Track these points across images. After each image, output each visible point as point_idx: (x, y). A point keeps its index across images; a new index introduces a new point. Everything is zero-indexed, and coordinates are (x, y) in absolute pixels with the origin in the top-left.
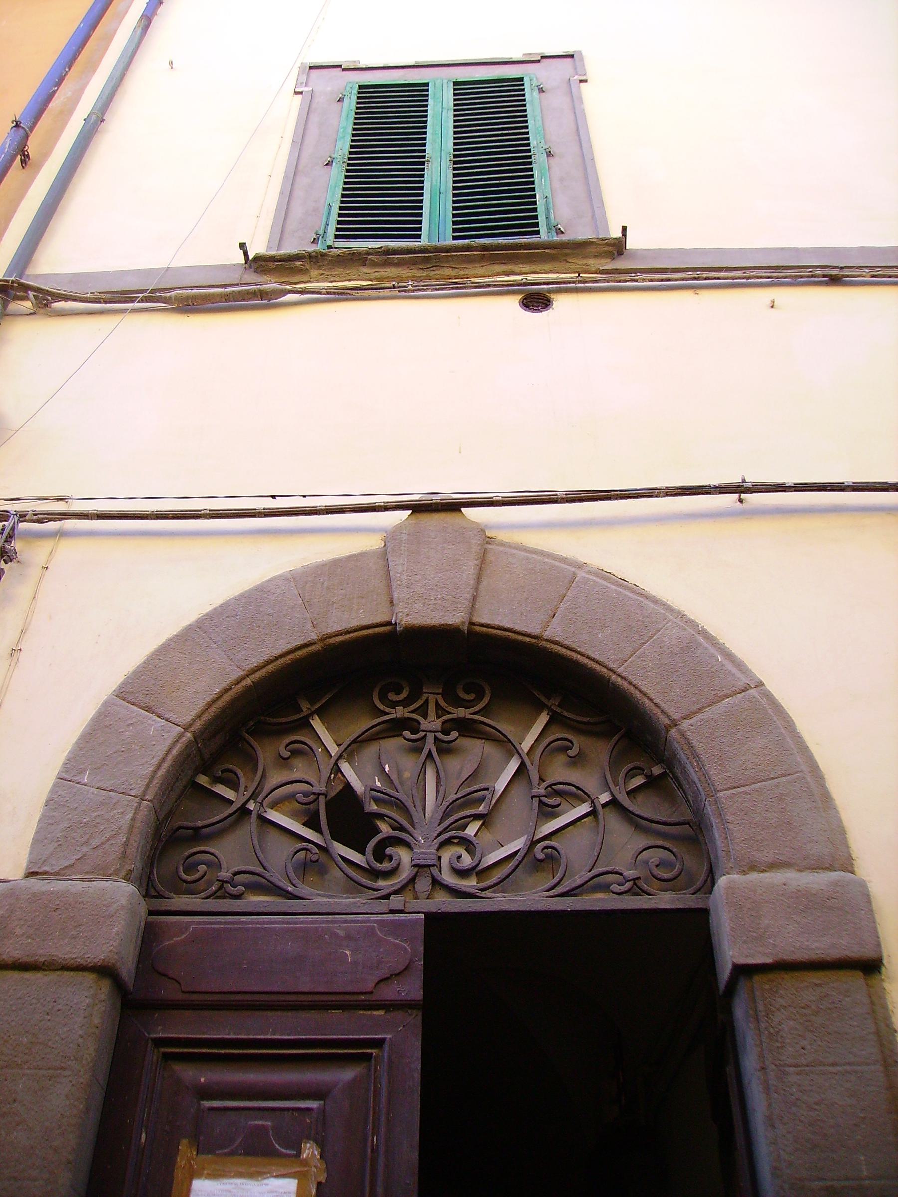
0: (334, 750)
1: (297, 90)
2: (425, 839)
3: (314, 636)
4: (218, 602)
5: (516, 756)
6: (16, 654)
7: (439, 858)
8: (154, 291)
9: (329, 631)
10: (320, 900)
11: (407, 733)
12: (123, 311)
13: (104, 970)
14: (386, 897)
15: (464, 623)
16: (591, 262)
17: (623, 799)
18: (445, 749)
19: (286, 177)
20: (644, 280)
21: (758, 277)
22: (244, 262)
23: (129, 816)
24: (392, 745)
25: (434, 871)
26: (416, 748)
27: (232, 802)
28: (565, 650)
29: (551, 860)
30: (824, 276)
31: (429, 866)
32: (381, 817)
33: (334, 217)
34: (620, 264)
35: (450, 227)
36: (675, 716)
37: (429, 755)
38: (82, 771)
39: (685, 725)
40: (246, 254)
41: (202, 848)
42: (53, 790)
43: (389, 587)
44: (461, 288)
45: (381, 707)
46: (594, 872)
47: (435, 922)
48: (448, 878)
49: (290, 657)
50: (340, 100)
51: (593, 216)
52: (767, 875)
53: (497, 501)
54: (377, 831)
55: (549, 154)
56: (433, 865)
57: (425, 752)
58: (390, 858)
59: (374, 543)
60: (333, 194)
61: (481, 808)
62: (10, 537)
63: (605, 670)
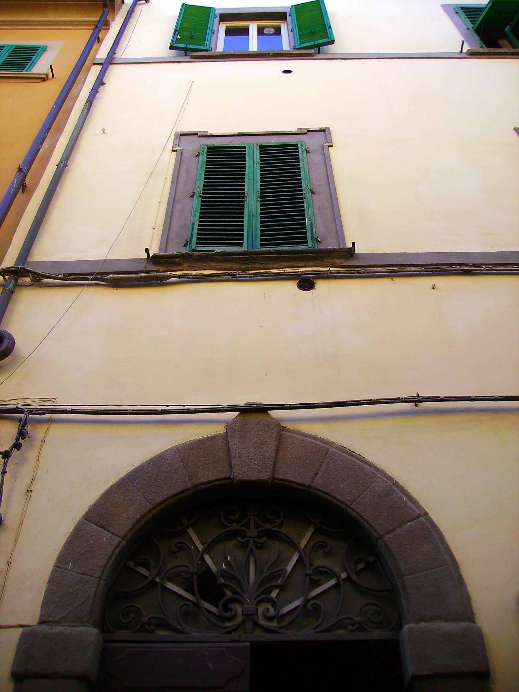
0: (200, 547)
1: (174, 149)
2: (250, 599)
3: (190, 485)
4: (138, 464)
5: (297, 551)
6: (29, 493)
7: (257, 610)
8: (98, 274)
9: (198, 482)
10: (195, 634)
11: (239, 538)
12: (83, 285)
13: (83, 678)
14: (230, 632)
15: (269, 479)
16: (336, 261)
17: (353, 576)
18: (261, 547)
19: (168, 204)
20: (364, 273)
21: (426, 271)
22: (147, 257)
23: (93, 590)
24: (231, 544)
25: (255, 617)
26: (244, 546)
27: (146, 577)
28: (323, 494)
29: (317, 609)
30: (461, 270)
31: (252, 615)
32: (226, 586)
33: (196, 231)
34: (351, 262)
35: (259, 238)
36: (381, 532)
37: (251, 550)
38: (67, 563)
39: (387, 537)
40: (148, 254)
41: (132, 604)
42: (52, 574)
43: (229, 456)
44: (266, 276)
45: (226, 523)
46: (340, 617)
47: (256, 647)
48: (262, 621)
49: (177, 497)
50: (198, 156)
51: (337, 232)
52: (429, 624)
53: (287, 407)
54: (225, 595)
55: (312, 193)
56: (254, 615)
57: (249, 549)
58: (232, 610)
59: (220, 429)
60: (195, 216)
61: (279, 582)
62: (25, 423)
63: (344, 506)
